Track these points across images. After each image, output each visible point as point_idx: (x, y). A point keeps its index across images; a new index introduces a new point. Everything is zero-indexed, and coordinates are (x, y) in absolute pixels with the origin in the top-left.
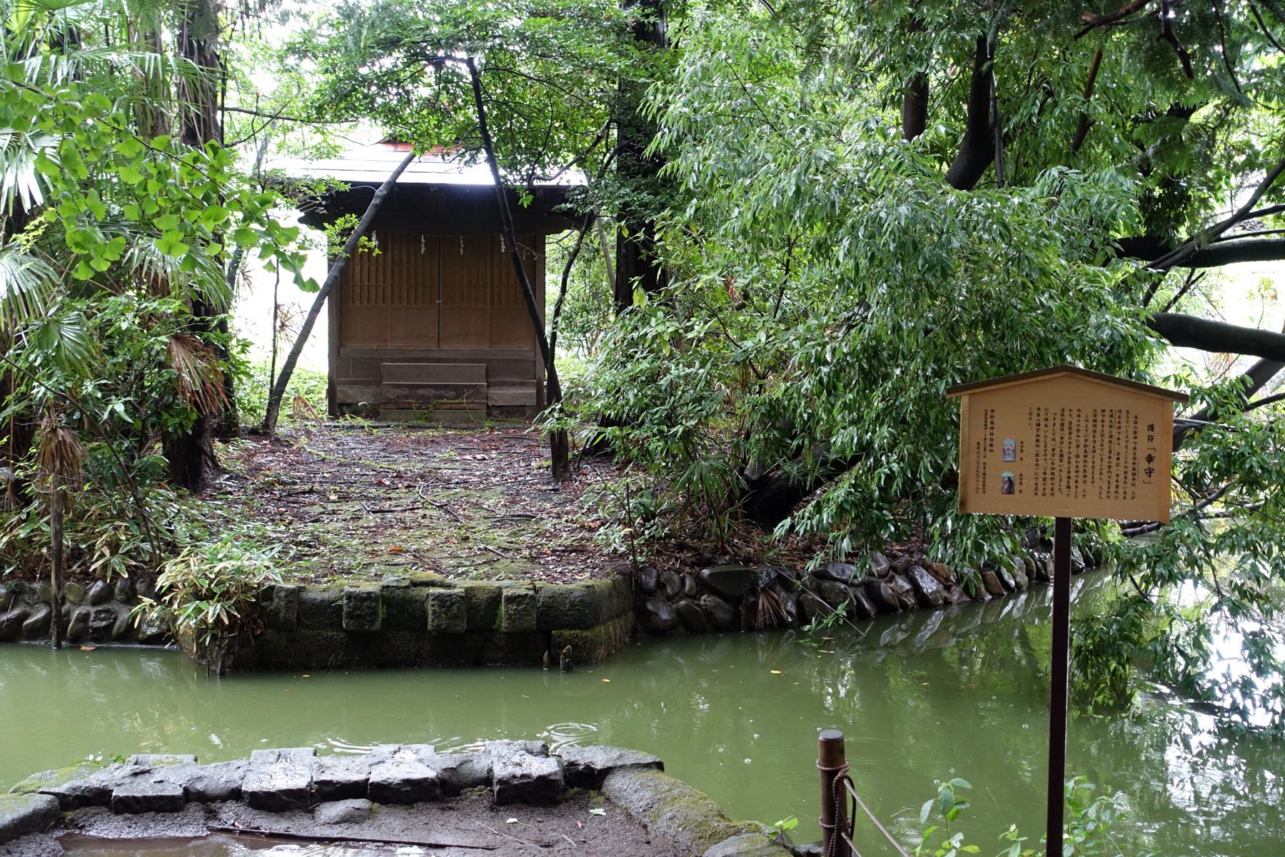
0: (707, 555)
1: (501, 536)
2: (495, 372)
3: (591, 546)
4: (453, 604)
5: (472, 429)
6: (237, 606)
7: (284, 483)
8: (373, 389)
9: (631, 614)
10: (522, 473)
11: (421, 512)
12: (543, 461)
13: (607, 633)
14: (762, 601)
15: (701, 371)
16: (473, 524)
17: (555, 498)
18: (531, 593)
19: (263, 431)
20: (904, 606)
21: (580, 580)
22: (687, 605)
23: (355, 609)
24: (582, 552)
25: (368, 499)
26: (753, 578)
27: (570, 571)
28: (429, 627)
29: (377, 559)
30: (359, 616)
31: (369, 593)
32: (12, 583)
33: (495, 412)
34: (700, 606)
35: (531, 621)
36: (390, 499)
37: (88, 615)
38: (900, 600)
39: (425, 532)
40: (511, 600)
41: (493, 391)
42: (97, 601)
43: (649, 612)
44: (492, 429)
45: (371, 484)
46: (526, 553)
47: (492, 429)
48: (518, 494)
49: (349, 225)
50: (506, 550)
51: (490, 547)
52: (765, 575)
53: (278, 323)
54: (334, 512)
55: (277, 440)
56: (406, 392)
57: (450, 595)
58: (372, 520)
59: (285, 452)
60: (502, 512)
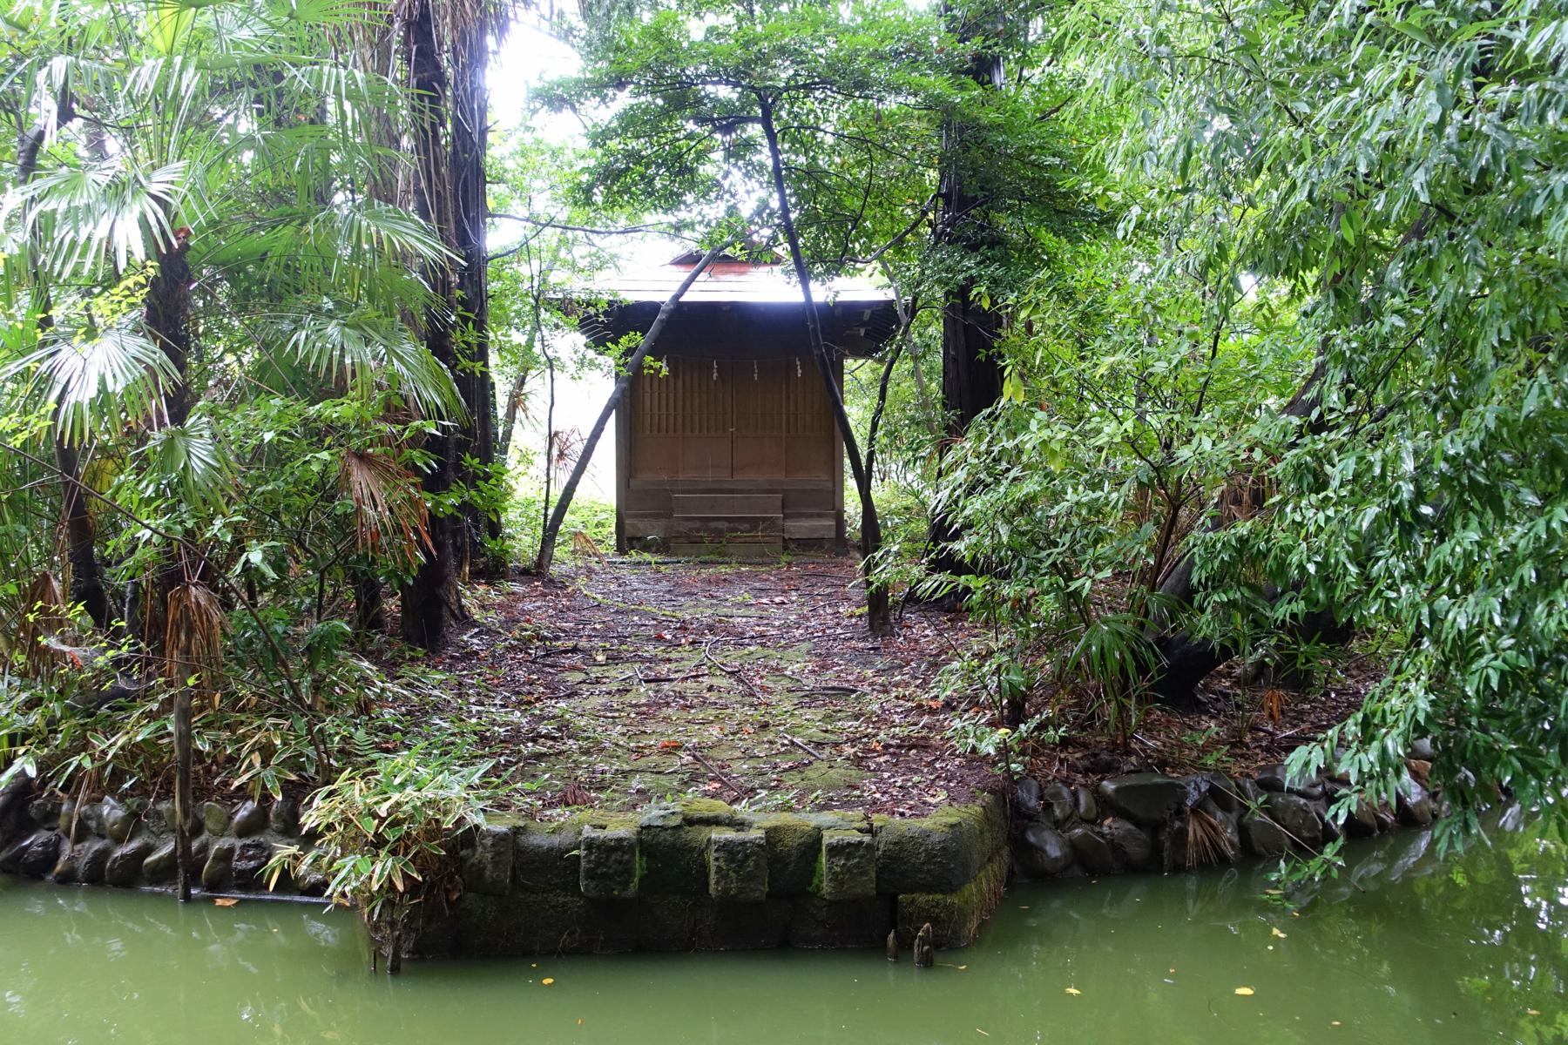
0: (1105, 756)
1: (811, 722)
2: (791, 505)
3: (936, 739)
4: (747, 857)
5: (767, 564)
6: (421, 861)
7: (543, 639)
8: (663, 522)
9: (1005, 852)
10: (831, 623)
11: (707, 681)
12: (853, 610)
13: (980, 891)
14: (1193, 830)
15: (1115, 495)
16: (774, 699)
17: (879, 663)
18: (867, 838)
19: (536, 571)
20: (1382, 825)
21: (940, 813)
22: (1085, 835)
23: (598, 864)
24: (925, 748)
25: (643, 660)
26: (1177, 791)
27: (915, 786)
28: (712, 887)
29: (642, 763)
30: (605, 876)
31: (620, 840)
32: (133, 802)
33: (792, 546)
34: (1103, 836)
35: (867, 884)
36: (669, 660)
37: (231, 850)
38: (1377, 818)
39: (711, 713)
40: (835, 850)
41: (789, 524)
42: (245, 830)
43: (1032, 847)
44: (789, 564)
45: (649, 639)
46: (849, 750)
47: (789, 564)
48: (828, 655)
49: (632, 345)
50: (819, 745)
51: (797, 740)
52: (1195, 787)
53: (555, 452)
54: (598, 681)
55: (551, 581)
56: (698, 524)
57: (743, 843)
58: (643, 693)
59: (557, 595)
60: (810, 682)
